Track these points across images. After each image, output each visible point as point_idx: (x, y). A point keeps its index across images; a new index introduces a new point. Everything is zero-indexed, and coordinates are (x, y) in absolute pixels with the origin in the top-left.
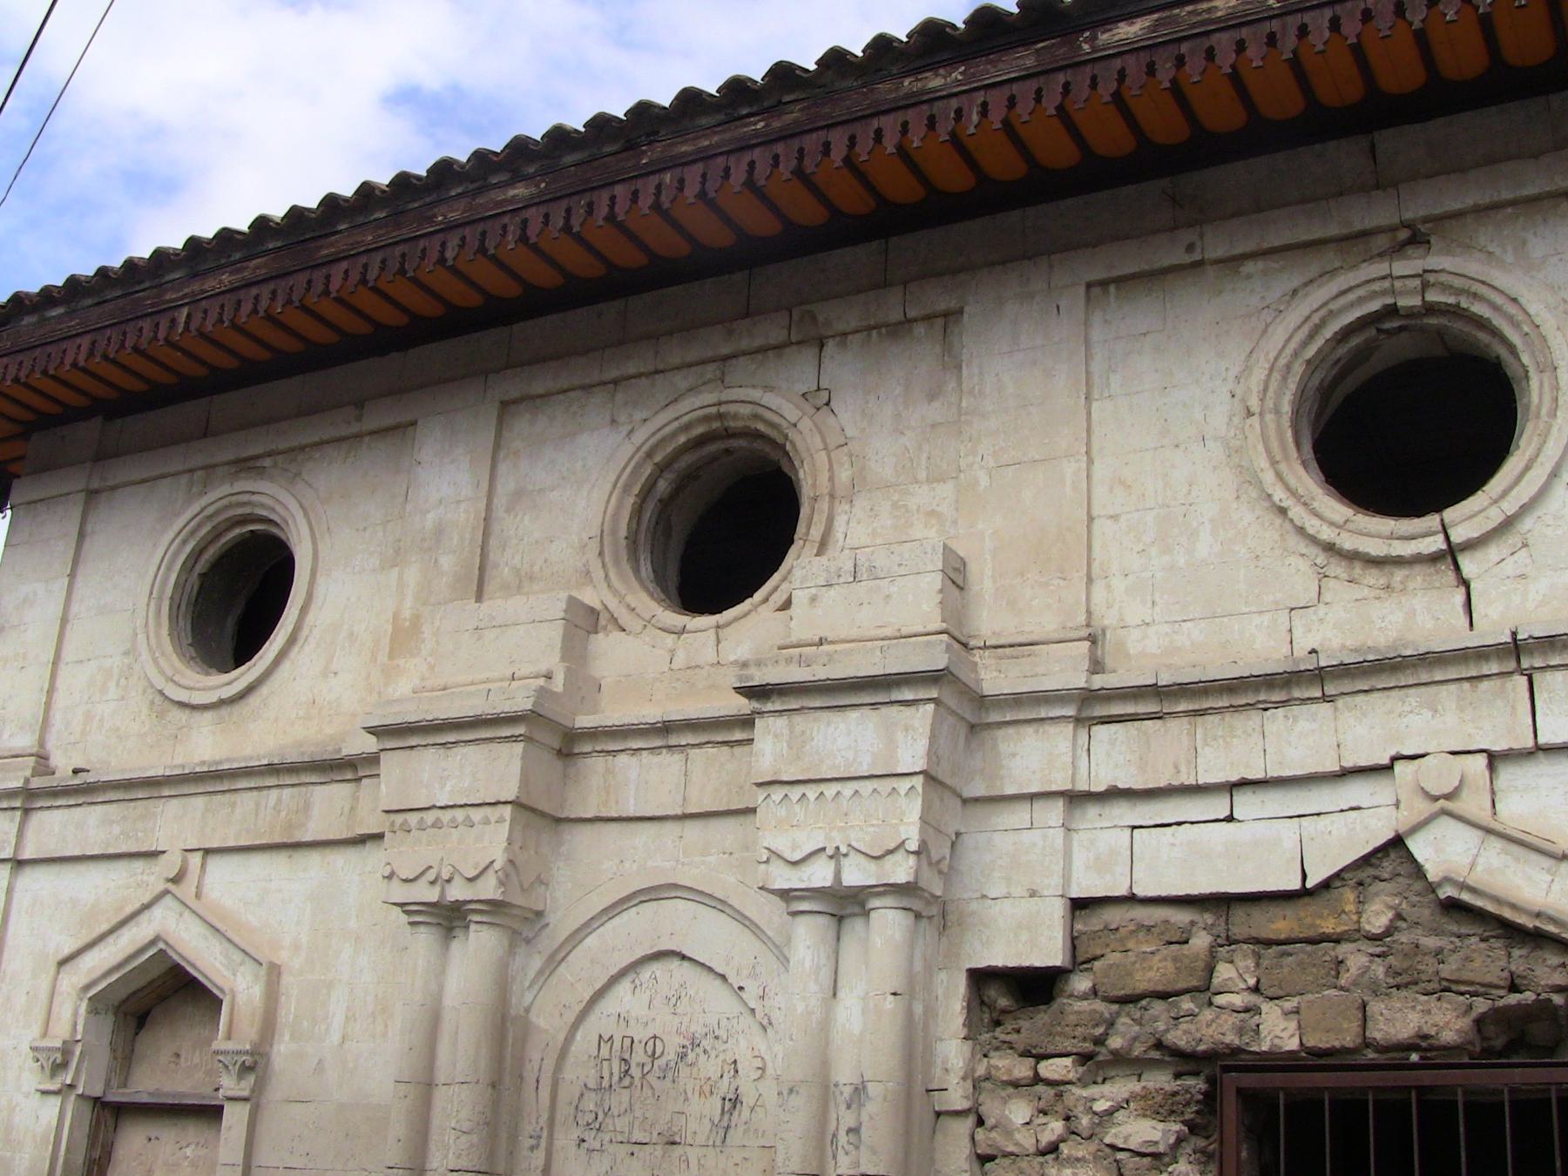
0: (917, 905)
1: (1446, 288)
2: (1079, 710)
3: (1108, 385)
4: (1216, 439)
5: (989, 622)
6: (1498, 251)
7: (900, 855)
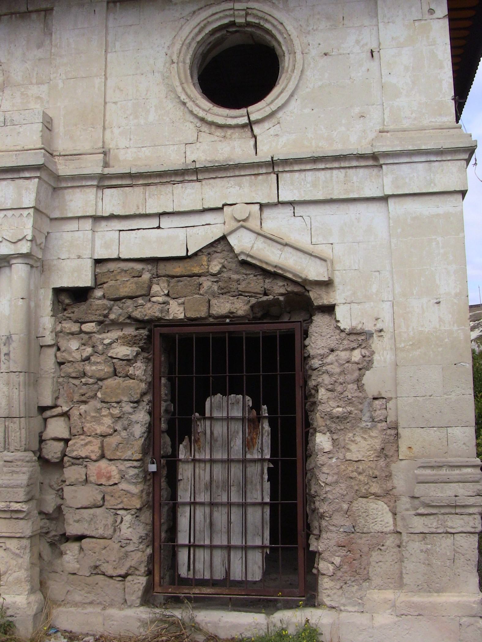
0: (31, 262)
1: (256, 16)
2: (99, 182)
3: (115, 47)
4: (159, 72)
5: (62, 145)
6: (277, 3)
7: (24, 242)
